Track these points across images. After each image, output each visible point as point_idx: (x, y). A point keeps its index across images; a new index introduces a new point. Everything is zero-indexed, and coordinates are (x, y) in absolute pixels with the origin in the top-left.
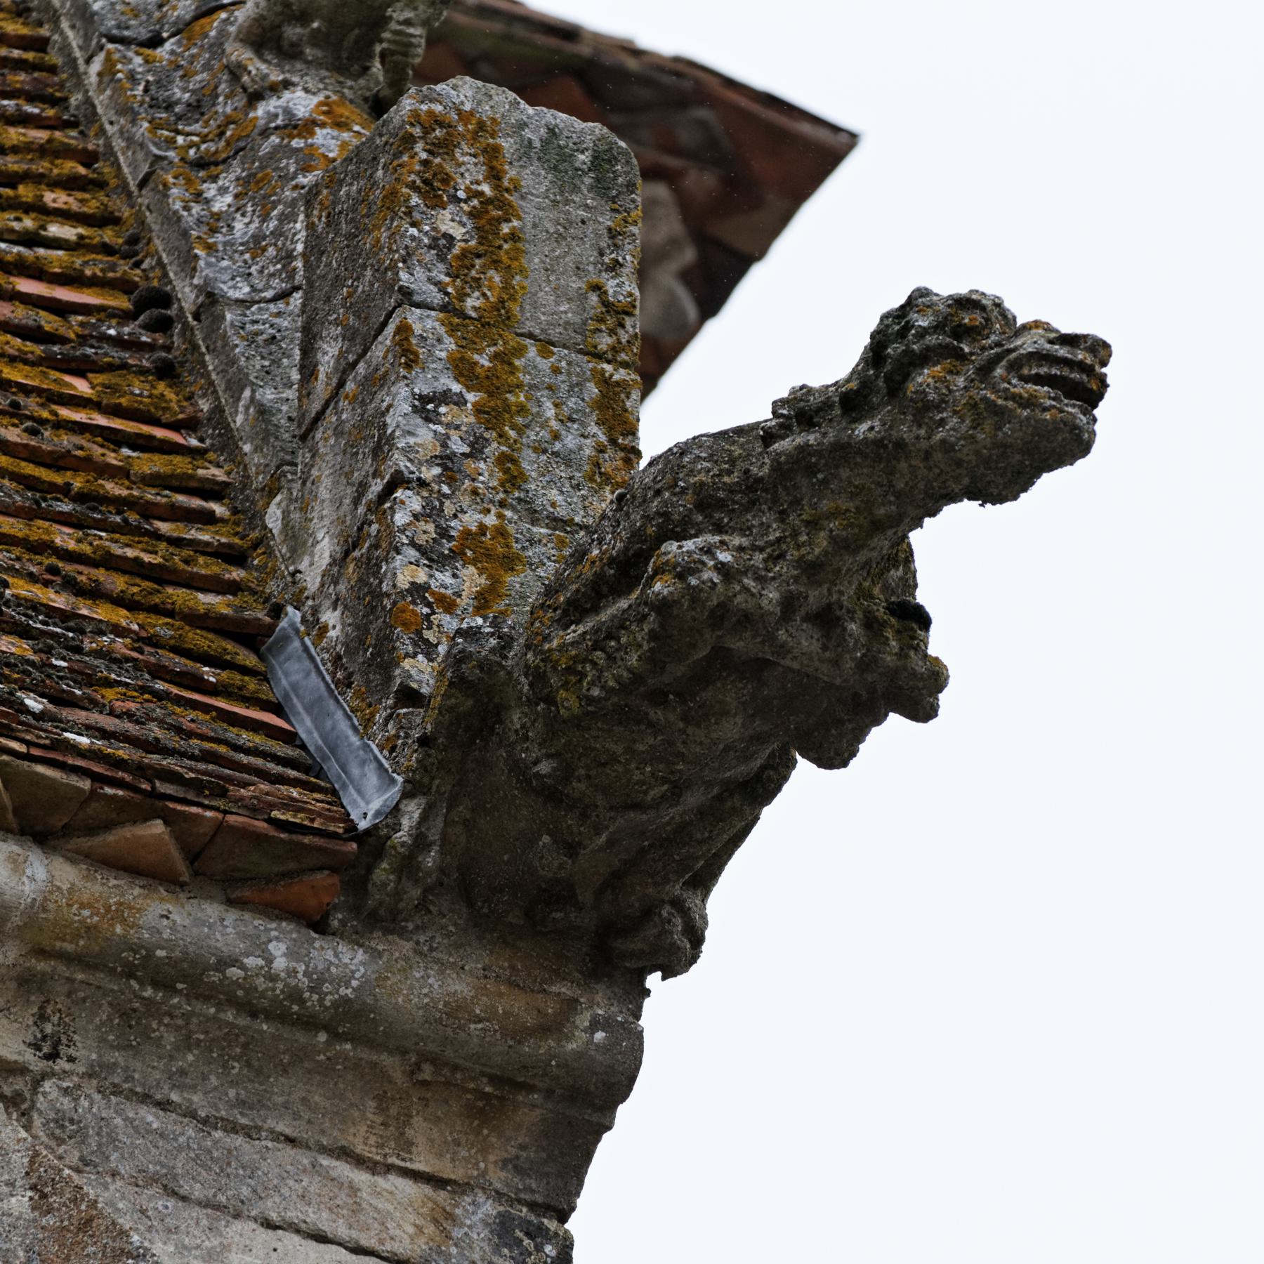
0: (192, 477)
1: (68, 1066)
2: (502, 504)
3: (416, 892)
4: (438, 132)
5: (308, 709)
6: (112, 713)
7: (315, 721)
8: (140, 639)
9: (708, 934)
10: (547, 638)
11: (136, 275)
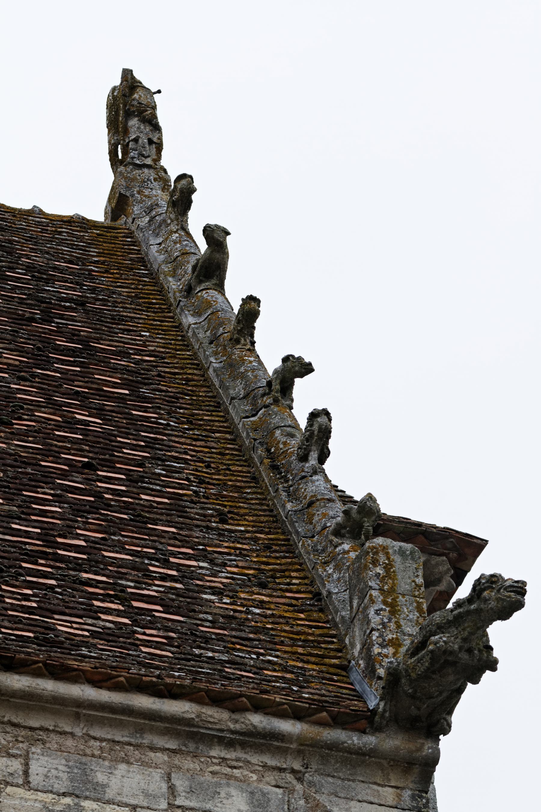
0: (329, 634)
1: (311, 770)
2: (397, 632)
3: (385, 722)
4: (375, 550)
5: (358, 684)
6: (313, 689)
7: (360, 686)
8: (319, 671)
9: (452, 725)
10: (407, 662)
11: (313, 589)
